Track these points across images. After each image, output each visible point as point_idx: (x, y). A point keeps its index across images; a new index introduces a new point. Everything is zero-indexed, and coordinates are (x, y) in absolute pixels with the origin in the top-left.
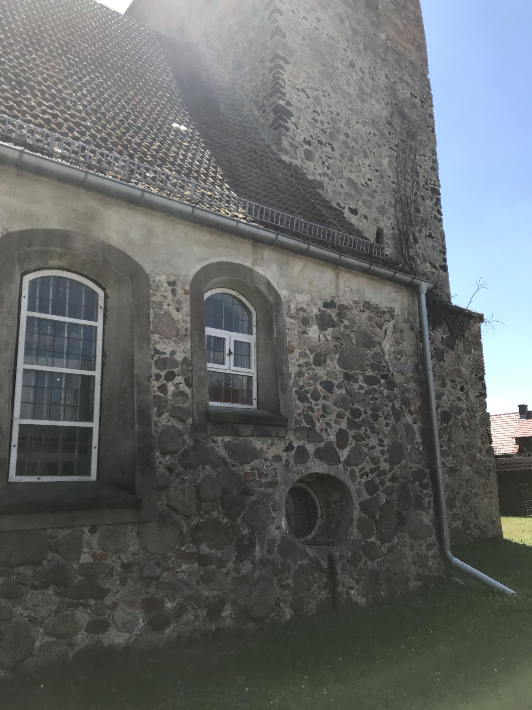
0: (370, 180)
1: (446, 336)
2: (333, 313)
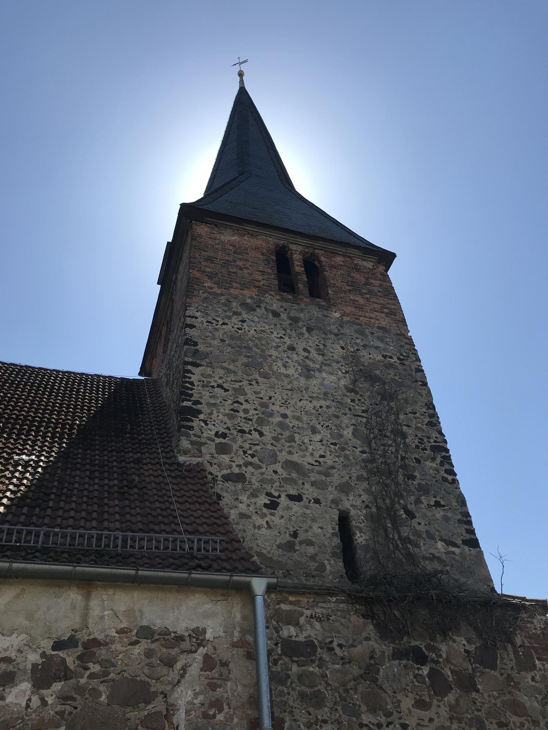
0: (322, 456)
1: (474, 646)
2: (70, 658)
